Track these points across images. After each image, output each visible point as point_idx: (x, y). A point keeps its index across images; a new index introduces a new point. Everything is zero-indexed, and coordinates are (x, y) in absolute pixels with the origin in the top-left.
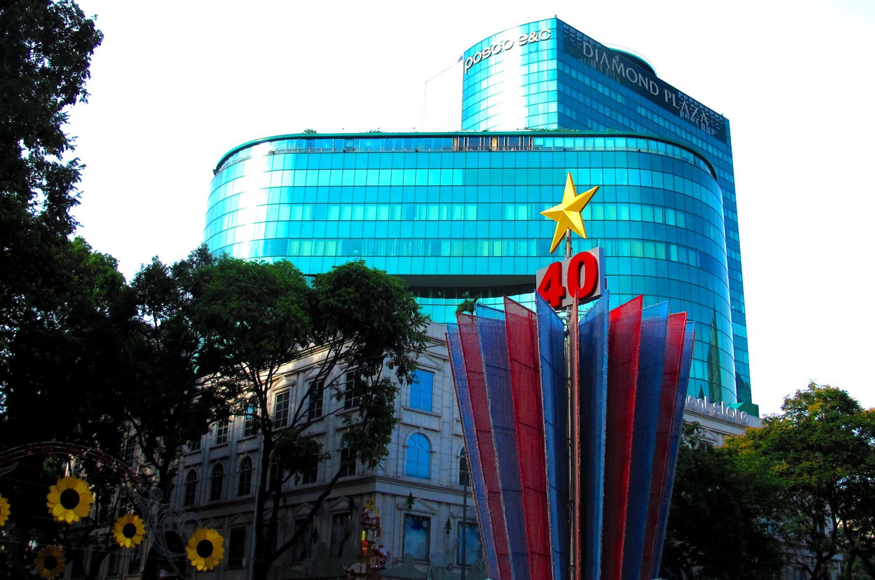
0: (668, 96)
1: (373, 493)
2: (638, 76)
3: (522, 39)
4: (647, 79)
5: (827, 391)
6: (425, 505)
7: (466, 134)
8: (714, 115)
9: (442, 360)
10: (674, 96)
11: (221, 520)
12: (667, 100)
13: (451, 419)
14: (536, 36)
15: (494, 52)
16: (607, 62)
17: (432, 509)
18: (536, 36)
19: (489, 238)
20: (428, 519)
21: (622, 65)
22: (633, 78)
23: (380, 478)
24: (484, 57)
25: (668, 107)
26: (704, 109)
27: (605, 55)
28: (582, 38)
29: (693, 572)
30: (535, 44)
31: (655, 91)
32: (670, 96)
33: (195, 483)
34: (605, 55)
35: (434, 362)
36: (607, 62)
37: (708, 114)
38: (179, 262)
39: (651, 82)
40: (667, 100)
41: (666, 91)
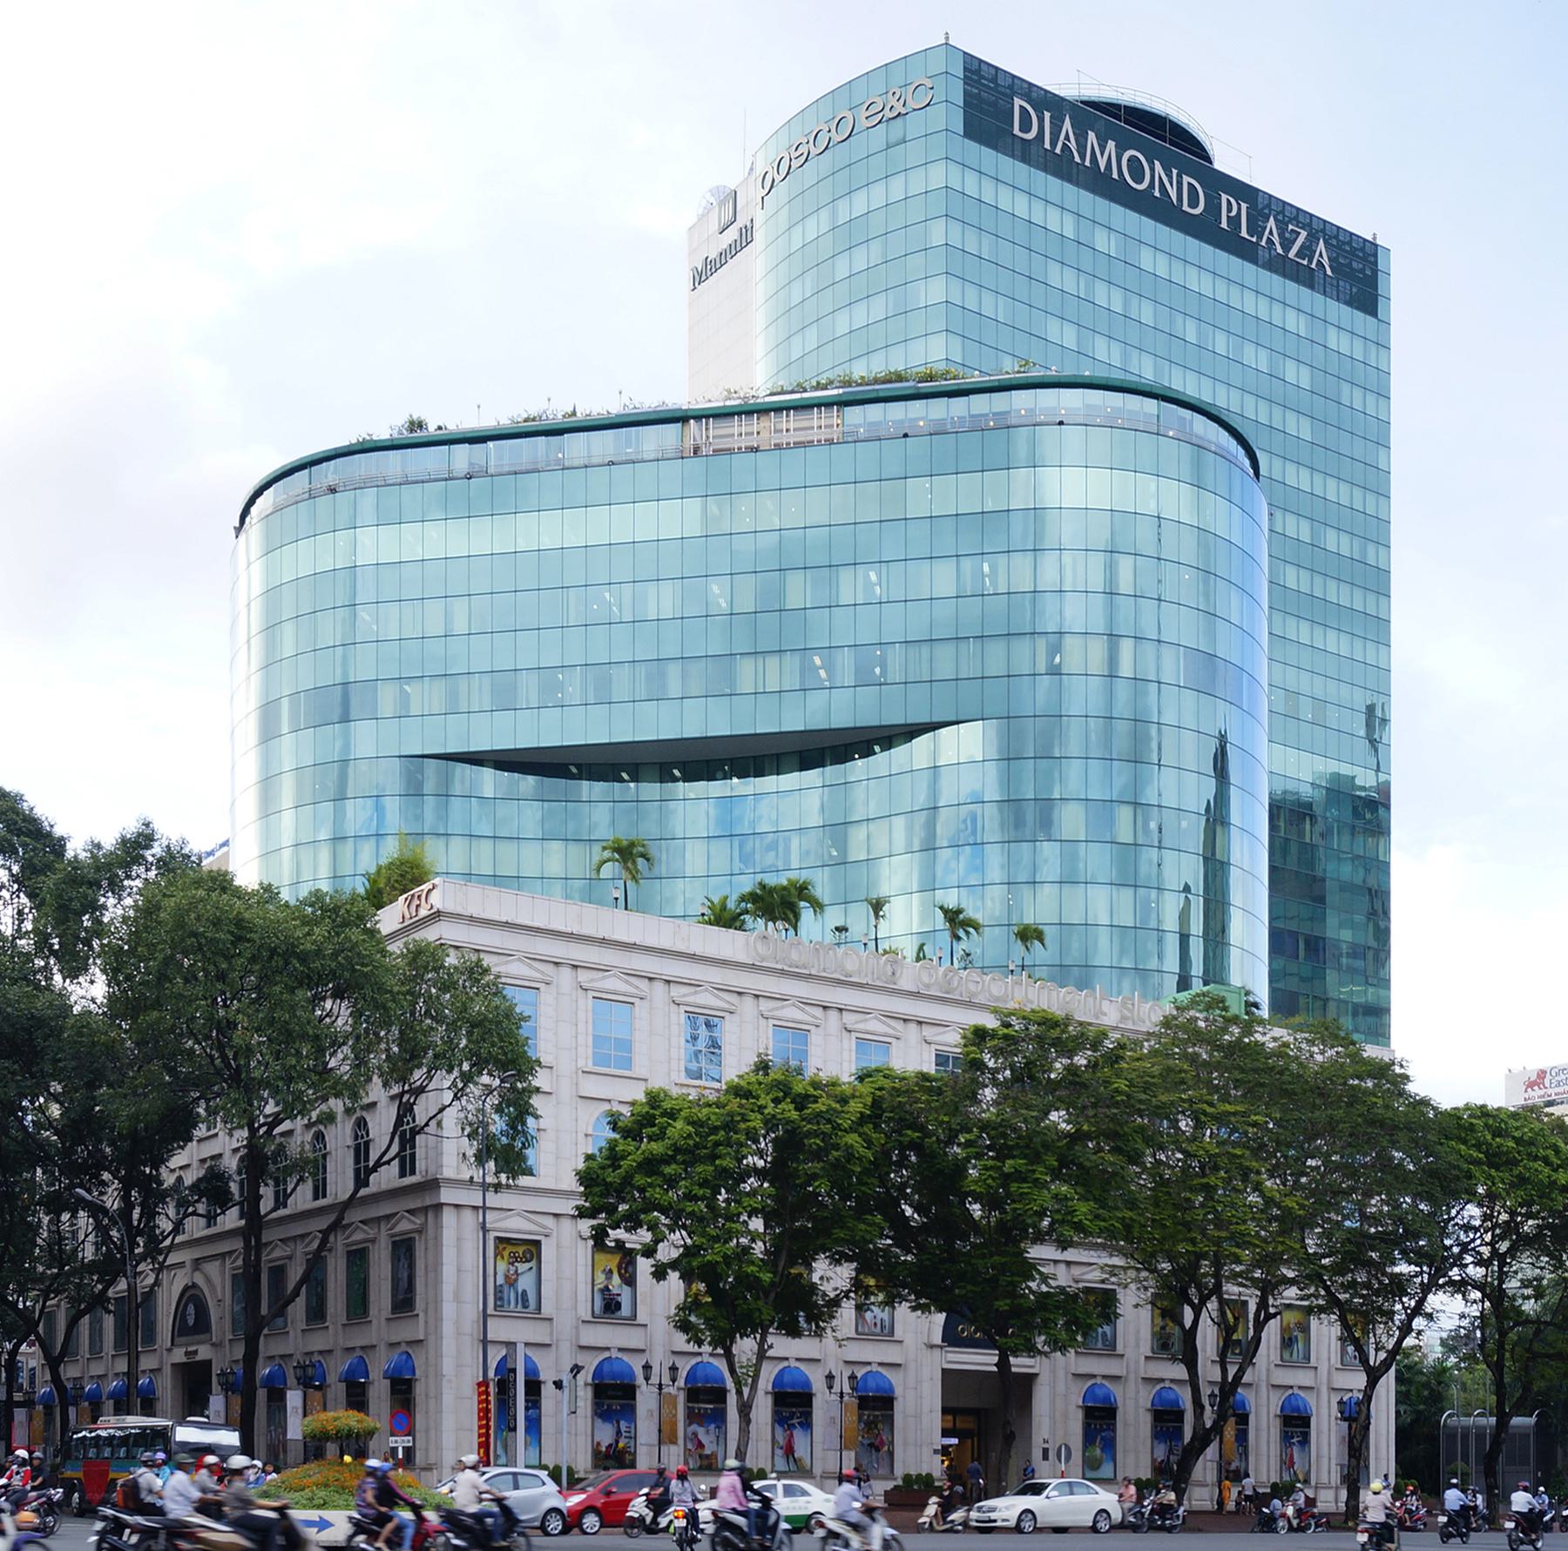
0: (1230, 209)
1: (438, 1207)
2: (1152, 170)
3: (873, 110)
4: (1175, 172)
5: (783, 1089)
6: (529, 1220)
7: (706, 413)
8: (1350, 243)
9: (552, 965)
10: (1244, 206)
11: (291, 1244)
12: (1224, 225)
13: (574, 1069)
14: (902, 101)
15: (814, 151)
16: (1073, 145)
17: (545, 1227)
18: (902, 101)
19: (756, 653)
20: (537, 1243)
21: (1111, 145)
22: (1138, 175)
23: (449, 1181)
24: (795, 164)
25: (1230, 243)
26: (1323, 231)
27: (1067, 124)
28: (1011, 87)
29: (903, 1310)
30: (899, 120)
31: (1194, 203)
32: (1234, 213)
33: (324, 1157)
34: (1067, 124)
35: (537, 970)
36: (1073, 145)
37: (1334, 242)
38: (58, 831)
39: (1186, 179)
40: (1224, 225)
41: (1224, 197)
